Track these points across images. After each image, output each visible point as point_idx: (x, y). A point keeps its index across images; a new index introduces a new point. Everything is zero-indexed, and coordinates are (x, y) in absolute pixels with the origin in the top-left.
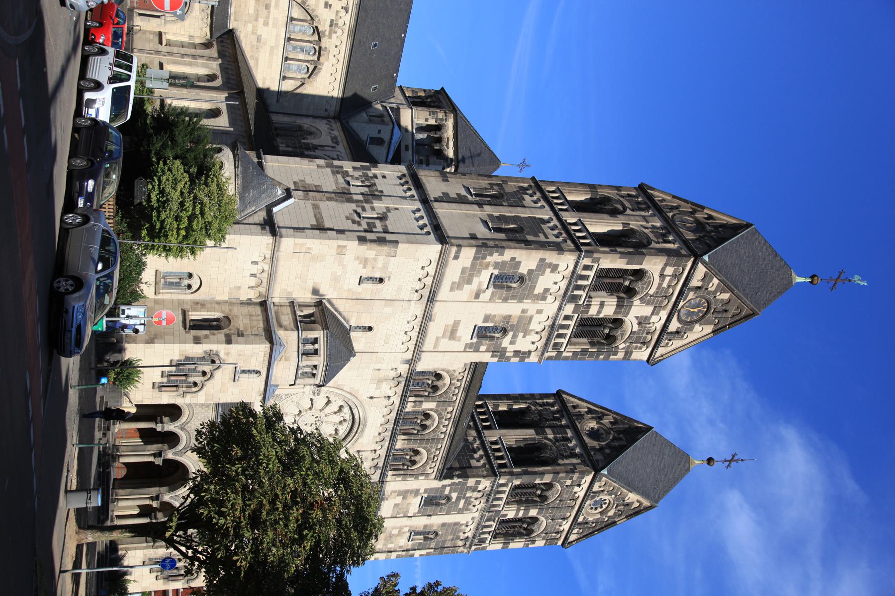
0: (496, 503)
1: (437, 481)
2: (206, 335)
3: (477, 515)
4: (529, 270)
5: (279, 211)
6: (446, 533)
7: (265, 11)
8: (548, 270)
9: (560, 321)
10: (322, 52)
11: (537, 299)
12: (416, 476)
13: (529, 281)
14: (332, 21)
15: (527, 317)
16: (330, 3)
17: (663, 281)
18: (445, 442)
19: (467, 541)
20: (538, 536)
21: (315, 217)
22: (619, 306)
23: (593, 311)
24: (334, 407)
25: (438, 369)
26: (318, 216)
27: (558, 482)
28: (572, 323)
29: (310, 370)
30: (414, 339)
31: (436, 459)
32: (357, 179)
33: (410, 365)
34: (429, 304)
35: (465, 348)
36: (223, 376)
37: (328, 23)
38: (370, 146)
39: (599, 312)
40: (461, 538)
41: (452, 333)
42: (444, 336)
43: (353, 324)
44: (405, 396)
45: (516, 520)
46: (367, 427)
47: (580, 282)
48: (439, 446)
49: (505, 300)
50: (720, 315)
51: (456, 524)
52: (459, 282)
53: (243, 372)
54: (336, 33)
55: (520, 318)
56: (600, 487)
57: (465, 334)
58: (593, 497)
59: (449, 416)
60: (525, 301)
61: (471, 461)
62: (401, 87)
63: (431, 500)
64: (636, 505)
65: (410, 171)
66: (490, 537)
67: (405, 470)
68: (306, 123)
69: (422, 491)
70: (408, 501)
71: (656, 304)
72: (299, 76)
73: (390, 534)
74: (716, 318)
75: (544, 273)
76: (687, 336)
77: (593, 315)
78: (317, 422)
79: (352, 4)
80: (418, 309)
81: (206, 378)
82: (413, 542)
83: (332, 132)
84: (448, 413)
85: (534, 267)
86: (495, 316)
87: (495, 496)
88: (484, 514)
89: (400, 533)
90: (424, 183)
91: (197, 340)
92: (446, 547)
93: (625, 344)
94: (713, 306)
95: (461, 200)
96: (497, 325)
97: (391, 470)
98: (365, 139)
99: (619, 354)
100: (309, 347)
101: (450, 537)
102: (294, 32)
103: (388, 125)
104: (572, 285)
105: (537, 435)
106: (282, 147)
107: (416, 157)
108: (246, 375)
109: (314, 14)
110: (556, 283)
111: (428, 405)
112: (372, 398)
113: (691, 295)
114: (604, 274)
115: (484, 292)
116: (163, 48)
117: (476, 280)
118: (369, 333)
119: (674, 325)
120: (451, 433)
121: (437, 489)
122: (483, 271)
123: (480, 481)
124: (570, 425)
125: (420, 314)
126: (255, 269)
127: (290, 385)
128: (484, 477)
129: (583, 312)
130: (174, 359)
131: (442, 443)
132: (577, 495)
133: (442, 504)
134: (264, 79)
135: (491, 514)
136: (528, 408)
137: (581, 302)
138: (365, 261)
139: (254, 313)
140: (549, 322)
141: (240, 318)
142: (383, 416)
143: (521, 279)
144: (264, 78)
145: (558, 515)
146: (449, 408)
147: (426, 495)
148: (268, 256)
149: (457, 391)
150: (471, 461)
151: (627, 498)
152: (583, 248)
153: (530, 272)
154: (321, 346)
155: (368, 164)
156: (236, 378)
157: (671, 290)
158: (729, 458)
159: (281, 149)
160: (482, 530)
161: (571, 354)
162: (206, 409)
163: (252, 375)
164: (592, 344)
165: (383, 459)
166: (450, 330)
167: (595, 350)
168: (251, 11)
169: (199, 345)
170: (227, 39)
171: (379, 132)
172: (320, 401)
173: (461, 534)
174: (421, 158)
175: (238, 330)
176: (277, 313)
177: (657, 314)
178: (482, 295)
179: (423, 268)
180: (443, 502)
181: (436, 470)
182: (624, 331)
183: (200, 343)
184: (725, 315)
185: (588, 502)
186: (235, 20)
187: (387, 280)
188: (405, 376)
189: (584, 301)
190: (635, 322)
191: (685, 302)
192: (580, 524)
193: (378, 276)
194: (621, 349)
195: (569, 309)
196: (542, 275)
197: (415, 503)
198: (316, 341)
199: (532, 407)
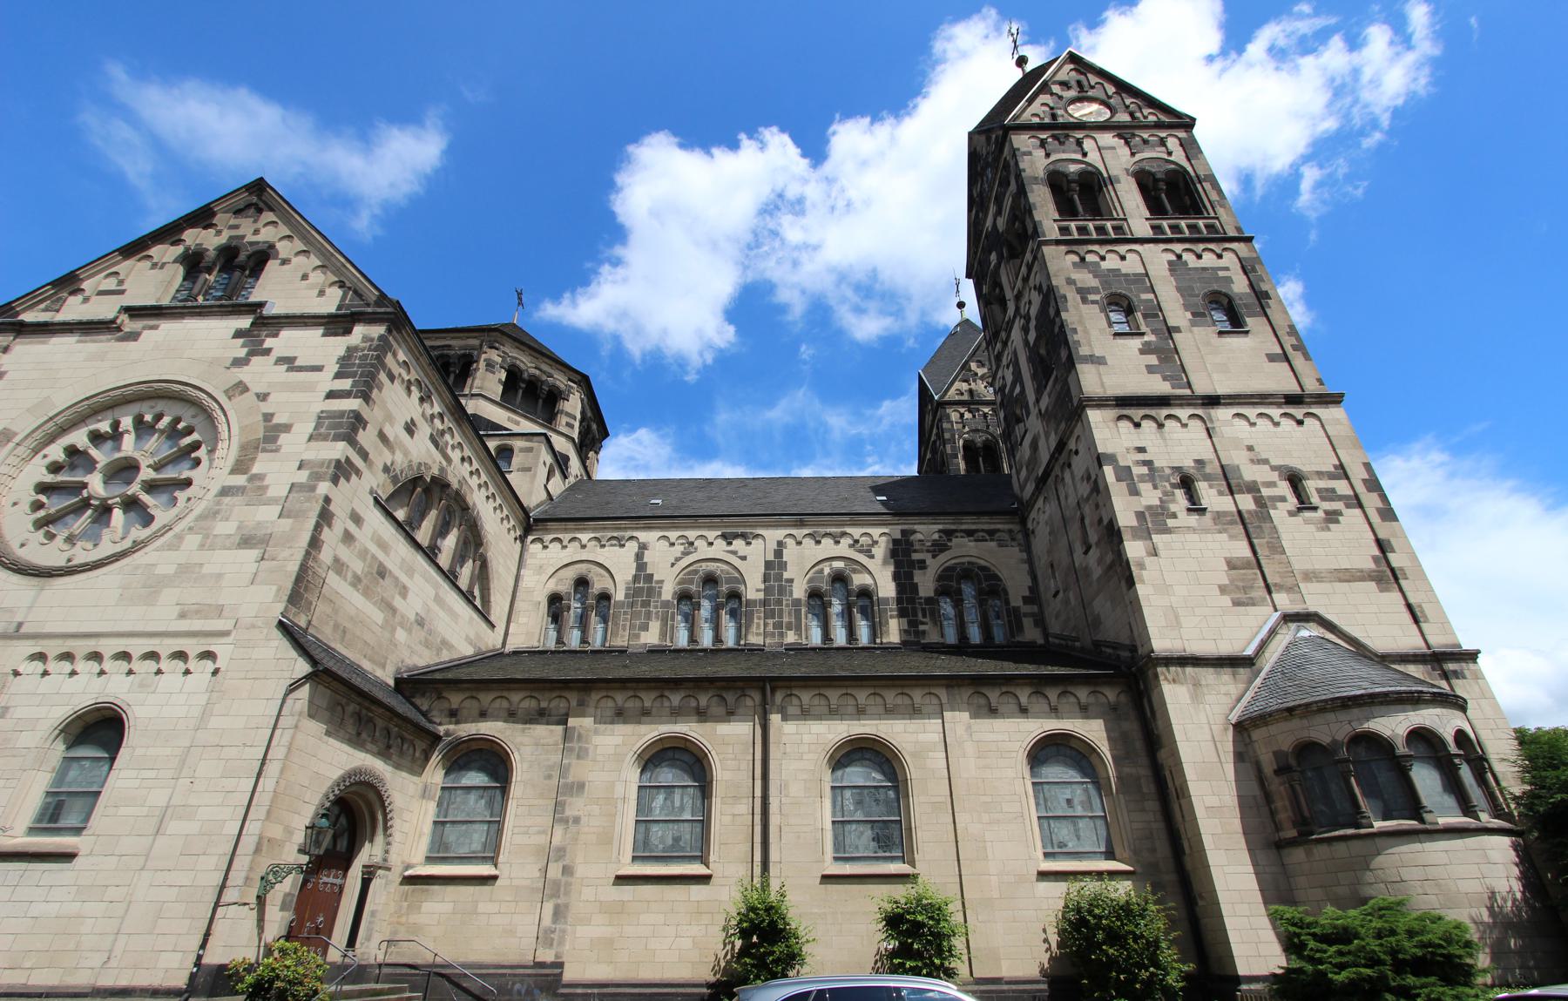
186: (383, 666)
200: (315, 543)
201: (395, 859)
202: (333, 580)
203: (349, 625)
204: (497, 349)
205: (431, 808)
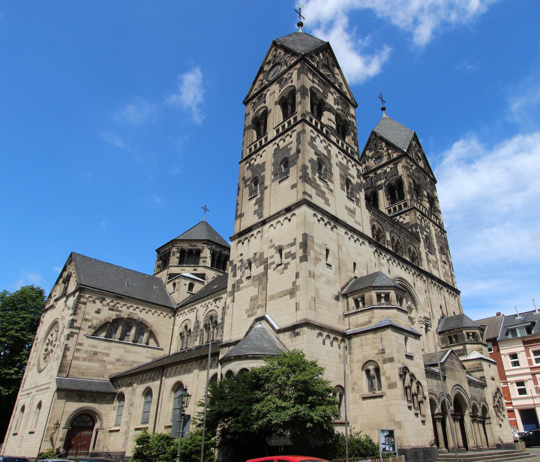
2: (386, 379)
7: (99, 355)
10: (131, 317)
14: (110, 309)
16: (97, 310)
20: (433, 194)
21: (282, 297)
37: (111, 312)
41: (352, 212)
42: (354, 218)
57: (352, 205)
62: (153, 275)
65: (236, 238)
80: (341, 231)
95: (260, 203)
98: (189, 295)
105: (383, 189)
109: (103, 321)
116: (122, 428)
124: (374, 172)
126: (328, 342)
134: (147, 357)
139: (360, 343)
141: (365, 353)
153: (316, 154)
168: (97, 365)
170: (118, 382)
171: (185, 285)
174: (202, 262)
176: (357, 326)
186: (103, 377)
187: (327, 247)
197: (431, 257)
200: (64, 356)
201: (104, 426)
204: (175, 246)
205: (116, 412)
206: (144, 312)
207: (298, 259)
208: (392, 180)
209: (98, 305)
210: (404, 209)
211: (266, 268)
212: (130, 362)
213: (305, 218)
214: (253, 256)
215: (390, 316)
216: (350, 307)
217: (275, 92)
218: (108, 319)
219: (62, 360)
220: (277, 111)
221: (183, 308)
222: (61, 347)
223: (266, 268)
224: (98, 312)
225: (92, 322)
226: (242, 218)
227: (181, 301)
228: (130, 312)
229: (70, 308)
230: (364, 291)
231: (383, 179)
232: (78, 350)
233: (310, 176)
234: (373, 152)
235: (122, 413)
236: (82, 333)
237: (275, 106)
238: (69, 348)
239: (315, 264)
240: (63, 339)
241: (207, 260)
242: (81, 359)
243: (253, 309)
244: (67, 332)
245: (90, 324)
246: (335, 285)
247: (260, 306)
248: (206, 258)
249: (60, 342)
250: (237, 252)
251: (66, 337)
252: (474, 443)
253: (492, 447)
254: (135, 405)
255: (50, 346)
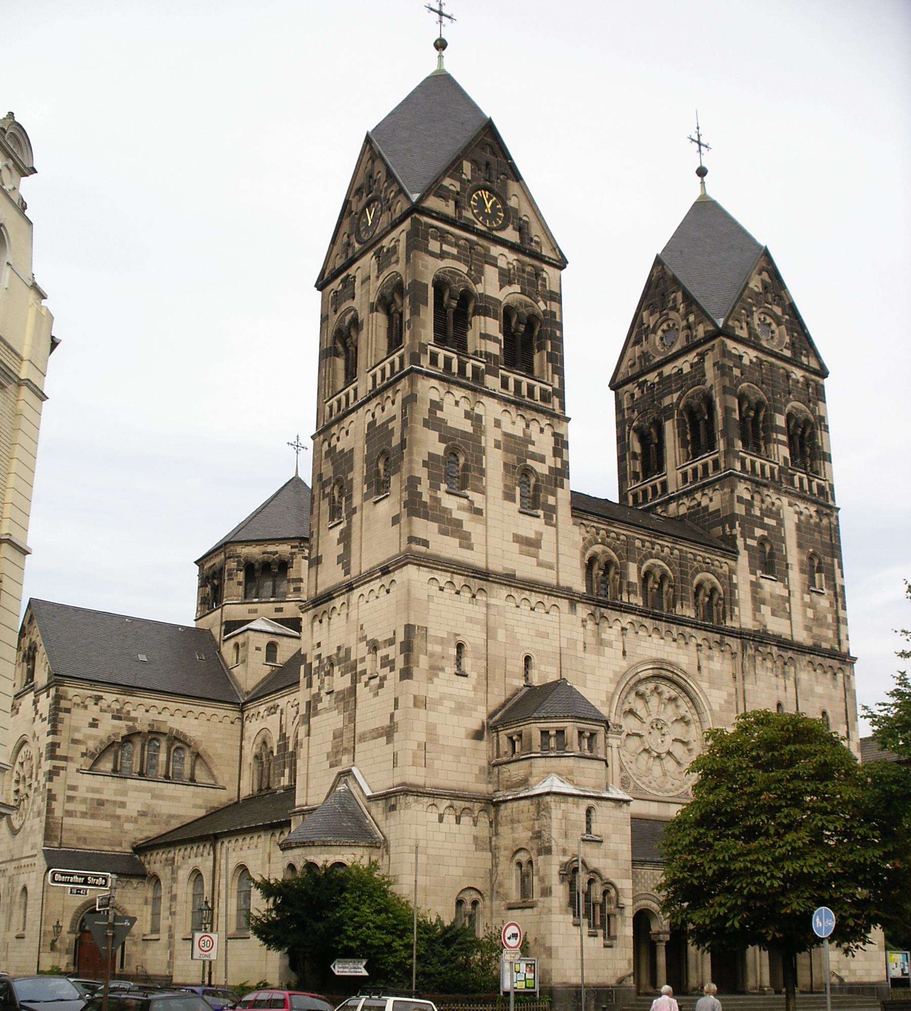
0: (768, 473)
1: (740, 557)
3: (785, 500)
4: (439, 441)
5: (369, 786)
6: (812, 542)
7: (107, 805)
8: (439, 414)
9: (510, 393)
10: (155, 729)
11: (481, 427)
12: (733, 587)
13: (454, 439)
14: (114, 717)
15: (506, 440)
17: (449, 254)
18: (685, 549)
19: (822, 511)
20: (813, 412)
21: (374, 738)
22: (485, 312)
23: (494, 349)
24: (638, 706)
25: (581, 562)
26: (374, 734)
27: (736, 386)
28: (512, 378)
29: (586, 740)
30: (540, 597)
31: (708, 560)
32: (322, 682)
33: (578, 601)
34: (491, 579)
35: (552, 525)
36: (595, 858)
37: (117, 722)
38: (278, 662)
39: (496, 340)
40: (817, 520)
41: (530, 544)
43: (522, 682)
44: (621, 606)
45: (791, 445)
46: (666, 658)
47: (455, 368)
48: (690, 556)
49: (482, 472)
50: (494, 173)
51: (798, 527)
52: (459, 537)
53: (589, 830)
54: (129, 711)
55: (507, 450)
56: (742, 328)
57: (531, 526)
58: (757, 337)
59: (647, 544)
60: (483, 444)
61: (710, 510)
63: (766, 565)
64: (765, 275)
66: (816, 480)
67: (724, 603)
68: (250, 750)
69: (753, 578)
70: (768, 597)
71: (481, 262)
72: (188, 760)
73: (813, 620)
74: (498, 178)
75: (443, 420)
76: (525, 215)
77: (500, 348)
78: (659, 727)
79: (91, 692)
80: (499, 595)
81: (598, 878)
82: (824, 587)
83: (261, 715)
84: (643, 546)
85: (435, 435)
86: (506, 486)
87: (758, 475)
88: (783, 490)
89: (812, 605)
90: (325, 590)
91: (546, 892)
92: (831, 541)
93: (539, 301)
94: (482, 182)
95: (345, 538)
96: (517, 482)
97: (725, 622)
99: (553, 310)
100: (553, 743)
101: (817, 536)
102: (131, 768)
103: (248, 638)
104: (459, 380)
106: (285, 781)
107: (291, 597)
108: (593, 825)
110: (457, 403)
111: (633, 574)
112: (624, 653)
113: (468, 214)
114: (441, 339)
115: (472, 502)
117: (457, 515)
118: (535, 660)
119: (510, 234)
120: (671, 540)
121: (750, 557)
122: (442, 505)
123: (738, 496)
124: (658, 371)
125: (504, 592)
126: (450, 818)
127: (607, 765)
128: (732, 491)
129: (496, 363)
130: (572, 921)
131: (686, 552)
132: (754, 360)
133: (771, 549)
134: (195, 806)
135: (783, 480)
136: (635, 431)
137: (483, 366)
138: (434, 669)
140: (512, 409)
142: (650, 636)
143: (452, 452)
144: (193, 807)
145: (782, 385)
146: (636, 544)
147: (759, 572)
148: (430, 801)
149: (613, 535)
150: (710, 510)
151: (756, 289)
152: (407, 367)
153: (442, 439)
154: (552, 726)
155: (302, 667)
156: (598, 839)
157: (462, 242)
158: (702, 141)
159: (287, 783)
160: (806, 492)
161: (556, 377)
162: (640, 877)
163: (593, 818)
164: (541, 347)
165: (710, 634)
166: (528, 548)
167: (549, 342)
168: (107, 824)
169: (553, 890)
171: (258, 649)
172: (630, 724)
173: (812, 521)
174: (292, 590)
175: (532, 838)
177: (496, 259)
178: (476, 505)
179: (441, 589)
180: (768, 548)
181: (723, 560)
182: (521, 303)
183: (550, 888)
184: (494, 165)
185: (764, 343)
186: (121, 845)
187: (458, 638)
188: (593, 607)
189: (480, 361)
190: (508, 289)
191: (476, 221)
192: (794, 353)
193: (453, 651)
194: (546, 306)
195: (492, 382)
196: (446, 423)
197: (770, 587)
198: (545, 733)
199: (634, 424)
200: (50, 811)
202: (68, 821)
203: (87, 836)
206: (179, 715)
207: (397, 673)
208: (692, 397)
209: (94, 711)
210: (712, 476)
211: (355, 681)
212: (165, 817)
213: (409, 592)
214: (335, 651)
215: (561, 772)
216: (502, 752)
217: (369, 278)
218: (113, 737)
219: (47, 818)
220: (374, 326)
221: (256, 703)
222: (42, 792)
223: (355, 681)
224: (94, 724)
225: (86, 744)
226: (320, 566)
227: (252, 687)
228: (154, 720)
229: (45, 719)
230: (521, 724)
231: (676, 391)
232: (70, 799)
233: (426, 498)
234: (657, 315)
235: (160, 910)
236: (72, 767)
237: (371, 315)
238: (55, 795)
239: (430, 680)
240: (42, 779)
241: (302, 585)
242: (78, 814)
243: (337, 752)
244: (47, 765)
245: (83, 749)
246: (475, 710)
247: (346, 750)
248: (301, 580)
249: (38, 783)
250: (312, 638)
251: (47, 776)
252: (756, 981)
253: (817, 988)
254: (179, 899)
255: (21, 787)
